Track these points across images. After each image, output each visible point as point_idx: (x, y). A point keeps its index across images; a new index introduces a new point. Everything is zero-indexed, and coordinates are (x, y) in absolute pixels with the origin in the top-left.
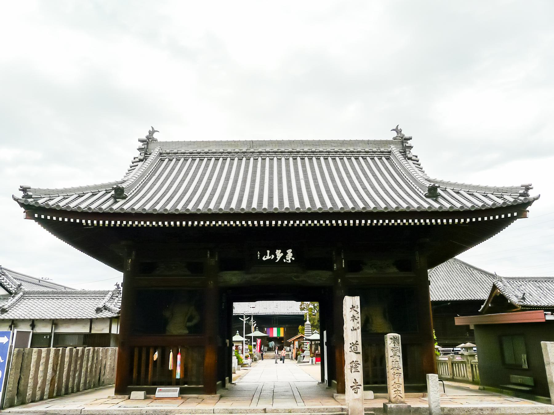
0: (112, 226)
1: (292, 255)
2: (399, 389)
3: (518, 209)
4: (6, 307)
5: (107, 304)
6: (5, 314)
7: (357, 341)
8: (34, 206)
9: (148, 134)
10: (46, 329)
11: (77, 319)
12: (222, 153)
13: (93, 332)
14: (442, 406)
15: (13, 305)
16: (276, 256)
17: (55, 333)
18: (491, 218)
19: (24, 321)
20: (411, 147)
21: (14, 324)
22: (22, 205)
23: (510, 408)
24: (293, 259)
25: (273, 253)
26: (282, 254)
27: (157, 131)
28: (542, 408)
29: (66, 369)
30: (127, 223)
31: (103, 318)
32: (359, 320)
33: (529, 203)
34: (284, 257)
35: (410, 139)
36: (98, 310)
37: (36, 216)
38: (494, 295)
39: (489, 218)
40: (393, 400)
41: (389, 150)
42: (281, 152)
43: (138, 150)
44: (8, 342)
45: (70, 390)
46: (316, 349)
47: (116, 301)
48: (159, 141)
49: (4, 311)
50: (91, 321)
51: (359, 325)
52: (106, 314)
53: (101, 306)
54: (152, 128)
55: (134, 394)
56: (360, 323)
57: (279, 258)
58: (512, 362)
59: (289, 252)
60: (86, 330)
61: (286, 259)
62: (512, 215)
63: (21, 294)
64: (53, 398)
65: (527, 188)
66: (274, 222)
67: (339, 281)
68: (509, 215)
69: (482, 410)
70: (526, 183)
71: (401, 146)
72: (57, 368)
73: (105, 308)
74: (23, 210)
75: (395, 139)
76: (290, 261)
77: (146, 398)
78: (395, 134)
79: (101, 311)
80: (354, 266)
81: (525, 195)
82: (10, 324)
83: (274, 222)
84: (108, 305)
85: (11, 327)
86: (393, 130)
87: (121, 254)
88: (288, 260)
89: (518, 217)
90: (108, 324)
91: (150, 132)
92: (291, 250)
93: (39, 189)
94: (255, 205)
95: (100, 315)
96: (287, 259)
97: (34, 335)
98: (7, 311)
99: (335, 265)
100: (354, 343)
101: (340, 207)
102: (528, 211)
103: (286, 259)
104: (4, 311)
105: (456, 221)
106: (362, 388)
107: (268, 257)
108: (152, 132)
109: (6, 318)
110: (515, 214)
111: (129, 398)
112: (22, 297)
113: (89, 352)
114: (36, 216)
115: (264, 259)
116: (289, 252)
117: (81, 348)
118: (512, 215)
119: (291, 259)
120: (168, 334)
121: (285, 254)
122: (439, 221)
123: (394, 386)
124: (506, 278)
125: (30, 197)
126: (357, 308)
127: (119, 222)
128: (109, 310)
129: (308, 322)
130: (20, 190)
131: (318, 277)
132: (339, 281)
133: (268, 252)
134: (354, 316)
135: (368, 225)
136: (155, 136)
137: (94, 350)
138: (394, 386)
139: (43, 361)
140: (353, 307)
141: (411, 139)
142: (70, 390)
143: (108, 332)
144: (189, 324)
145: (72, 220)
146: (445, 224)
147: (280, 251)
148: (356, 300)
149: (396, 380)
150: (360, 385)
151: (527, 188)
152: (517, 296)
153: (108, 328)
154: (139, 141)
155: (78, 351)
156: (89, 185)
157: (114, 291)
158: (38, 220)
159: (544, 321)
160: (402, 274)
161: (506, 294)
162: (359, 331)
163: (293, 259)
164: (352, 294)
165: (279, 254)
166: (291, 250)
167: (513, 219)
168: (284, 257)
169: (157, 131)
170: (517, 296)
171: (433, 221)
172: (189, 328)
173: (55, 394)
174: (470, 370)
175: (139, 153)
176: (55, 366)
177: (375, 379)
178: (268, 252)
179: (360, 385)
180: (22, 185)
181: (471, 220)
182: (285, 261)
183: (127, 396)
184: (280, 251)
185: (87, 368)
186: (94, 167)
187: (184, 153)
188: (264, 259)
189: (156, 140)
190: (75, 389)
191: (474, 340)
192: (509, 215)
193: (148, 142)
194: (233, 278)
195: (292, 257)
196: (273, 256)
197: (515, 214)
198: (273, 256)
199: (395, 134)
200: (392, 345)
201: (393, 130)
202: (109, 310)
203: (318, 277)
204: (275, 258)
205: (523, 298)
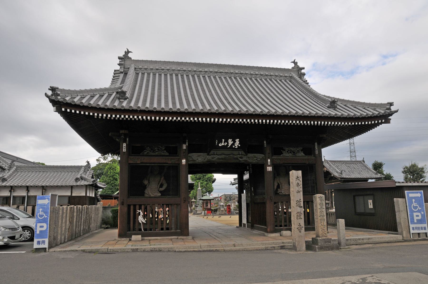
0: (161, 120)
4: (6, 177)
5: (82, 175)
6: (6, 182)
8: (63, 102)
9: (124, 53)
10: (23, 193)
11: (62, 186)
12: (179, 70)
13: (73, 195)
14: (347, 238)
15: (10, 176)
16: (228, 143)
17: (13, 197)
18: (363, 123)
19: (21, 187)
20: (304, 74)
23: (378, 238)
24: (239, 145)
25: (226, 141)
26: (232, 142)
27: (131, 52)
28: (395, 237)
30: (173, 118)
31: (82, 185)
32: (301, 186)
33: (391, 115)
34: (233, 144)
35: (304, 68)
36: (77, 180)
39: (358, 123)
40: (320, 235)
41: (291, 75)
42: (220, 72)
46: (207, 206)
47: (88, 173)
48: (132, 59)
49: (4, 180)
50: (72, 187)
51: (301, 189)
52: (83, 183)
53: (79, 176)
54: (128, 50)
55: (134, 237)
57: (230, 145)
58: (362, 211)
59: (237, 140)
60: (69, 194)
62: (378, 121)
63: (15, 167)
65: (391, 104)
66: (216, 120)
67: (269, 160)
69: (363, 239)
70: (391, 101)
71: (297, 73)
73: (82, 178)
75: (293, 68)
76: (237, 147)
77: (142, 240)
78: (293, 65)
79: (79, 180)
81: (389, 109)
82: (10, 189)
83: (268, 121)
84: (83, 175)
85: (11, 191)
86: (292, 62)
87: (117, 140)
90: (85, 189)
91: (125, 52)
92: (238, 140)
94: (155, 105)
95: (78, 183)
98: (7, 180)
100: (299, 200)
101: (185, 108)
102: (390, 119)
104: (4, 180)
105: (162, 118)
106: (303, 229)
107: (223, 144)
108: (127, 52)
109: (7, 185)
110: (383, 121)
112: (16, 170)
115: (220, 145)
116: (237, 140)
117: (66, 206)
118: (378, 121)
119: (238, 146)
120: (146, 195)
121: (234, 142)
122: (256, 121)
124: (330, 161)
125: (59, 95)
127: (225, 120)
128: (85, 180)
129: (199, 188)
130: (49, 89)
132: (269, 160)
133: (223, 140)
134: (298, 184)
135: (275, 124)
136: (130, 55)
137: (77, 207)
139: (65, 215)
140: (298, 177)
143: (84, 195)
144: (161, 189)
145: (87, 113)
146: (205, 121)
147: (231, 140)
149: (322, 223)
151: (391, 104)
152: (337, 172)
155: (63, 209)
156: (97, 88)
157: (86, 166)
159: (395, 186)
160: (307, 157)
161: (331, 170)
162: (302, 193)
163: (239, 145)
164: (297, 169)
165: (230, 142)
166: (238, 140)
167: (382, 123)
168: (233, 144)
169: (131, 52)
170: (337, 172)
171: (252, 121)
172: (160, 192)
177: (309, 222)
178: (223, 140)
180: (52, 86)
182: (233, 147)
183: (128, 239)
184: (231, 140)
186: (93, 75)
187: (152, 69)
188: (220, 145)
189: (131, 58)
193: (125, 59)
196: (226, 143)
197: (383, 121)
198: (226, 143)
199: (293, 65)
201: (292, 62)
202: (85, 180)
204: (228, 145)
205: (341, 173)
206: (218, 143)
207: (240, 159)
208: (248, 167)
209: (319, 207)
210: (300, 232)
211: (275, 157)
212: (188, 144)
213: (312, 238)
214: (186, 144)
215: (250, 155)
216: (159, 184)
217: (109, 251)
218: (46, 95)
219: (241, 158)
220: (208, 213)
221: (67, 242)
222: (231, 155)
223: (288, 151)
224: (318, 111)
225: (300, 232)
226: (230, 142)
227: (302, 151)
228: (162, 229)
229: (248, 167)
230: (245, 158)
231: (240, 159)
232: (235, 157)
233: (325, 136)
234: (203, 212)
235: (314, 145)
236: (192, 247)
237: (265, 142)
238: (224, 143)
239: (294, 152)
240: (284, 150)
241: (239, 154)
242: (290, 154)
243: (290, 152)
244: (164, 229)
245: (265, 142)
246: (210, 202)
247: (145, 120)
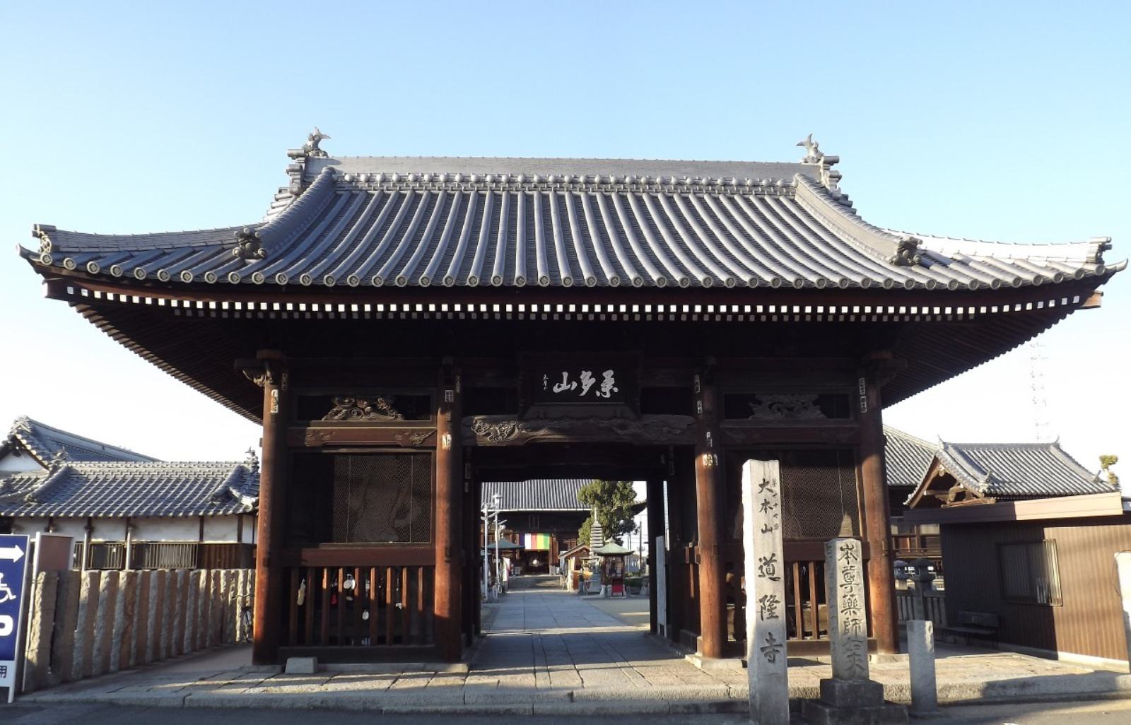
1: (613, 381)
2: (858, 652)
3: (1078, 290)
7: (773, 555)
13: (206, 542)
16: (580, 384)
21: (54, 525)
22: (39, 269)
24: (616, 390)
25: (575, 377)
26: (593, 380)
29: (152, 613)
34: (596, 386)
37: (70, 291)
38: (933, 476)
43: (288, 172)
44: (22, 559)
45: (163, 653)
51: (778, 521)
56: (780, 516)
57: (586, 389)
59: (608, 375)
60: (193, 539)
61: (600, 391)
62: (1070, 300)
64: (128, 668)
67: (708, 435)
68: (1064, 302)
72: (133, 612)
74: (41, 278)
76: (608, 395)
80: (735, 406)
88: (605, 394)
89: (1079, 306)
90: (235, 526)
92: (611, 373)
93: (76, 233)
96: (603, 390)
97: (91, 546)
99: (699, 403)
103: (600, 391)
107: (565, 386)
111: (283, 670)
113: (923, 470)
114: (70, 291)
115: (556, 390)
116: (608, 375)
118: (1070, 300)
119: (611, 391)
121: (600, 379)
123: (848, 646)
126: (774, 484)
131: (662, 428)
132: (708, 435)
133: (565, 375)
138: (848, 646)
141: (837, 162)
142: (163, 653)
143: (234, 541)
144: (400, 523)
147: (590, 373)
148: (772, 469)
150: (781, 645)
153: (236, 533)
154: (290, 155)
158: (75, 300)
162: (778, 534)
163: (616, 390)
165: (587, 380)
166: (611, 373)
167: (1071, 308)
168: (596, 386)
173: (132, 662)
174: (921, 607)
175: (291, 178)
176: (130, 608)
178: (565, 375)
179: (781, 645)
181: (977, 310)
182: (598, 394)
183: (278, 668)
184: (590, 373)
185: (196, 610)
188: (556, 390)
190: (173, 650)
191: (431, 566)
192: (1064, 302)
194: (494, 431)
195: (614, 386)
196: (574, 385)
197: (1076, 300)
200: (844, 561)
203: (662, 428)
204: (579, 389)
206: (551, 385)
207: (619, 431)
208: (662, 457)
209: (840, 579)
210: (773, 661)
211: (728, 424)
212: (462, 387)
213: (823, 682)
214: (453, 388)
215: (651, 419)
216: (395, 510)
217: (187, 703)
218: (26, 254)
219: (623, 427)
220: (614, 590)
221: (113, 672)
222: (591, 421)
223: (770, 406)
224: (869, 275)
225: (773, 661)
226: (587, 380)
227: (815, 403)
228: (381, 640)
229: (662, 457)
230: (634, 428)
231: (619, 431)
232: (605, 424)
233: (887, 355)
234: (603, 587)
235: (856, 384)
236: (437, 700)
237: (697, 379)
238: (569, 382)
239: (791, 409)
240: (760, 403)
241: (615, 417)
242: (779, 415)
243: (779, 410)
244: (388, 639)
245: (697, 379)
246: (623, 560)
247: (332, 316)
